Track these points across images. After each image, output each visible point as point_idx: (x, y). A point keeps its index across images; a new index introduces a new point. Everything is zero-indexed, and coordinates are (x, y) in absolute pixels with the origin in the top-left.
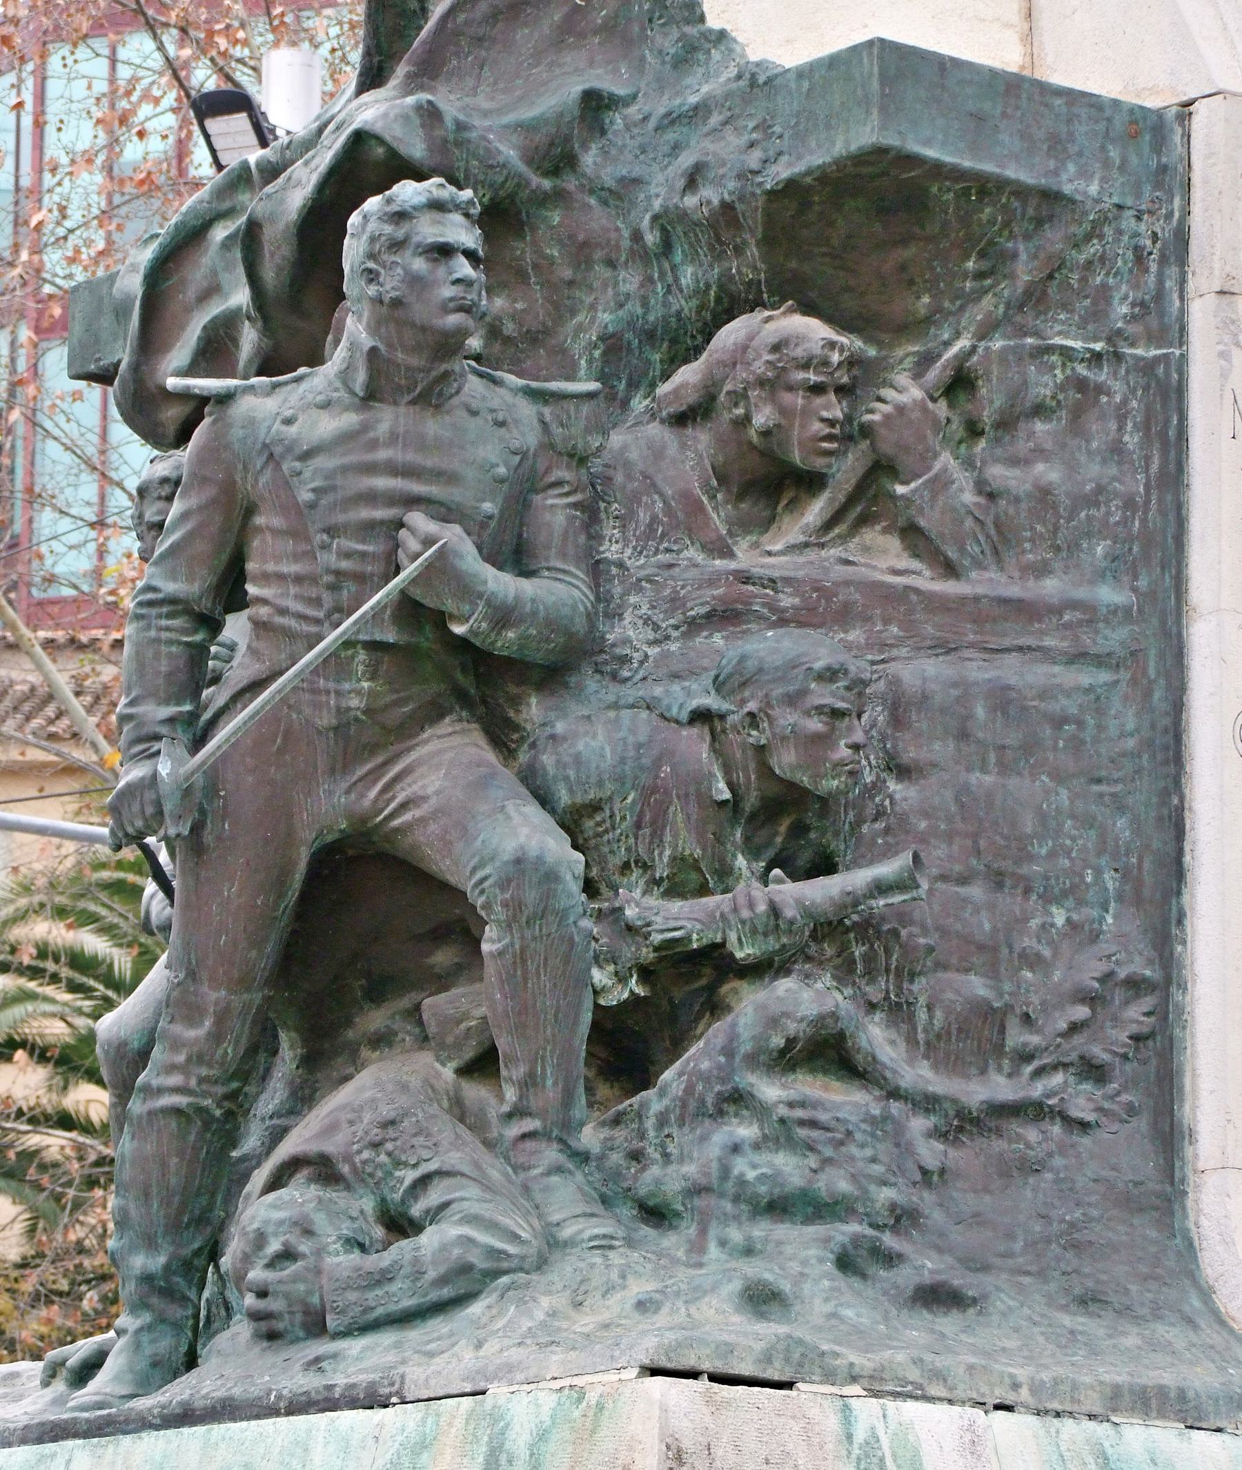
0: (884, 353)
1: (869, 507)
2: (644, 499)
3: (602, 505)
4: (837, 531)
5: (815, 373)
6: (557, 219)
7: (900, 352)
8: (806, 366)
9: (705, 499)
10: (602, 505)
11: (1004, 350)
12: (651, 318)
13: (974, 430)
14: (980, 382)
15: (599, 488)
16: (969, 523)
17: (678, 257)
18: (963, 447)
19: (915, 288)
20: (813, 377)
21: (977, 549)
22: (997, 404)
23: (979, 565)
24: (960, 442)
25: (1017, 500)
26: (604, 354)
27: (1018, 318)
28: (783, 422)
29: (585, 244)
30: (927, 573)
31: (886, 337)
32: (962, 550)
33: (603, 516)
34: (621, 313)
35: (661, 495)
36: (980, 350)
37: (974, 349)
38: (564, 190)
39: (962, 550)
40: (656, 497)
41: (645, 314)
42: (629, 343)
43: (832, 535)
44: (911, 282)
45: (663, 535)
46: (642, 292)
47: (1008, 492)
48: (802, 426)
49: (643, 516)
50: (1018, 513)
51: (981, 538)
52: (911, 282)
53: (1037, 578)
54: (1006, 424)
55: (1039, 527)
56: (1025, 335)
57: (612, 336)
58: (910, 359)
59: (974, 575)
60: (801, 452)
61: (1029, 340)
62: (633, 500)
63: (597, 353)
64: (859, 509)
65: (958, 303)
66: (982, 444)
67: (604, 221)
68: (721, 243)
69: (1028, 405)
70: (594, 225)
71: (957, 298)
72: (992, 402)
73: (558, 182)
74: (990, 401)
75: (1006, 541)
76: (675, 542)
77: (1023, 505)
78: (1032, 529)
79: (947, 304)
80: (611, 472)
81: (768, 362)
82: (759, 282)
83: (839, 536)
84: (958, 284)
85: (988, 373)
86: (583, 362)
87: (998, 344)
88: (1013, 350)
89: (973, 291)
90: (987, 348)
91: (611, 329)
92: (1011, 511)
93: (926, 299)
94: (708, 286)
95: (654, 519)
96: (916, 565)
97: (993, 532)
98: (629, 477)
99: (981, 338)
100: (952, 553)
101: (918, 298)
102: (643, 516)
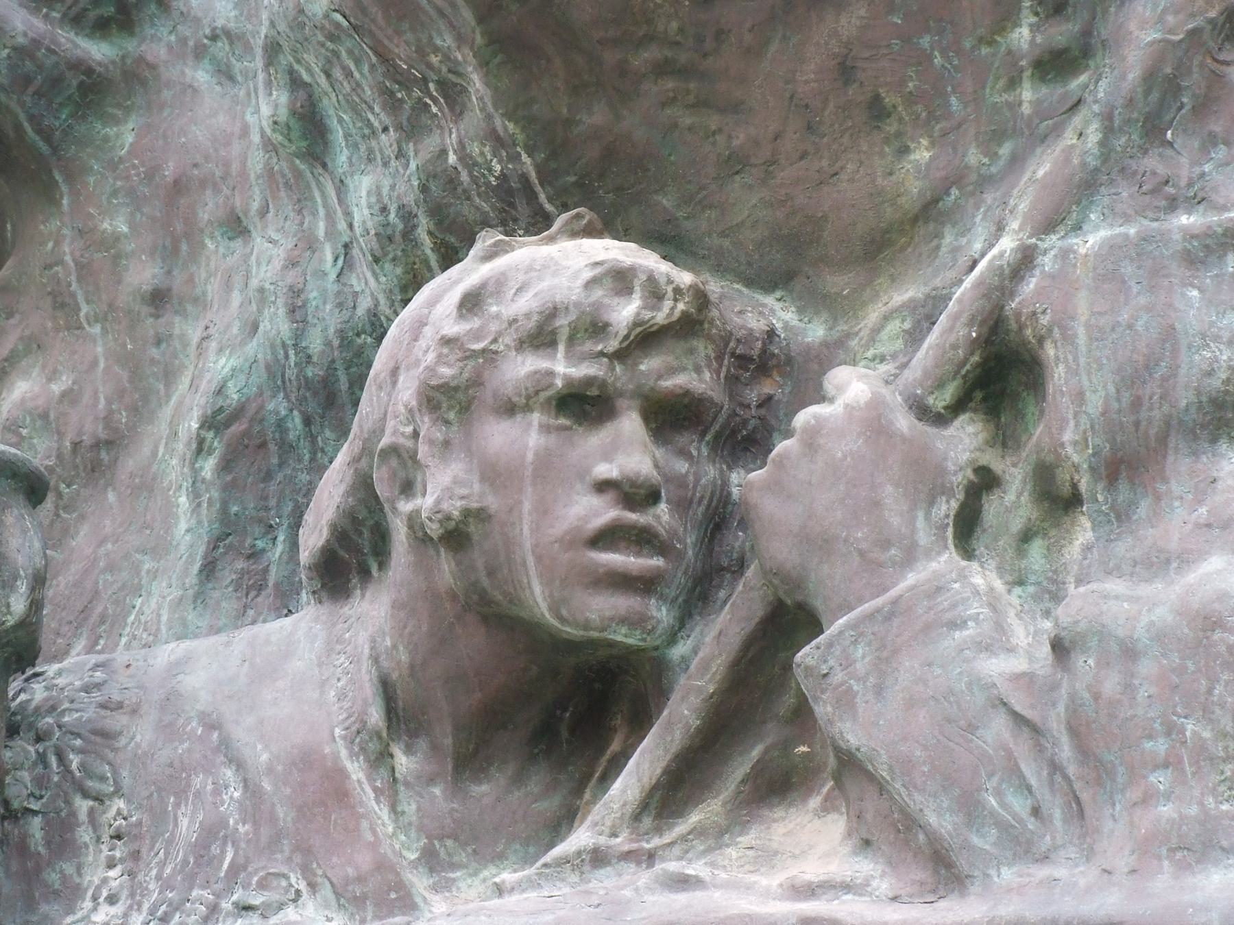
0: (842, 327)
1: (786, 746)
2: (197, 781)
3: (83, 806)
4: (695, 818)
5: (570, 357)
6: (129, 138)
7: (873, 315)
8: (541, 337)
9: (356, 771)
10: (83, 806)
11: (1113, 249)
12: (315, 343)
13: (1058, 501)
14: (1050, 351)
15: (75, 761)
16: (998, 729)
17: (342, 158)
18: (1037, 548)
19: (891, 127)
20: (563, 368)
21: (1019, 805)
22: (1095, 403)
23: (1021, 846)
24: (1026, 537)
25: (1130, 652)
26: (226, 465)
27: (1152, 163)
28: (492, 502)
29: (179, 187)
30: (883, 886)
31: (837, 282)
32: (970, 808)
33: (84, 835)
34: (252, 348)
35: (239, 765)
36: (1047, 262)
37: (1026, 260)
38: (141, 60)
39: (970, 808)
40: (229, 773)
41: (298, 335)
42: (280, 425)
43: (681, 828)
44: (877, 111)
45: (235, 870)
46: (292, 277)
47: (1103, 634)
48: (543, 510)
49: (187, 825)
50: (1129, 688)
51: (1029, 770)
52: (877, 111)
53: (1183, 867)
54: (1130, 462)
55: (1190, 727)
56: (1173, 205)
57: (238, 413)
58: (894, 326)
59: (1007, 875)
60: (547, 582)
61: (1185, 220)
62: (175, 782)
63: (208, 466)
64: (756, 752)
65: (1005, 150)
66: (1083, 532)
67: (222, 119)
68: (406, 82)
69: (1184, 398)
70: (199, 134)
71: (998, 136)
72: (1080, 397)
73: (131, 45)
74: (1076, 404)
75: (1100, 773)
76: (263, 885)
77: (1146, 668)
78: (1171, 730)
79: (974, 156)
80: (116, 721)
81: (447, 341)
82: (524, 178)
83: (699, 832)
84: (996, 96)
85: (1063, 324)
86: (183, 499)
87: (1095, 237)
88: (1141, 249)
89: (1041, 112)
90: (1065, 253)
91: (233, 395)
92: (1111, 685)
93: (922, 154)
94: (407, 216)
95: (213, 832)
96: (864, 867)
97: (1066, 752)
98: (169, 731)
99: (1049, 225)
100: (940, 818)
101: (904, 151)
102: (187, 825)
